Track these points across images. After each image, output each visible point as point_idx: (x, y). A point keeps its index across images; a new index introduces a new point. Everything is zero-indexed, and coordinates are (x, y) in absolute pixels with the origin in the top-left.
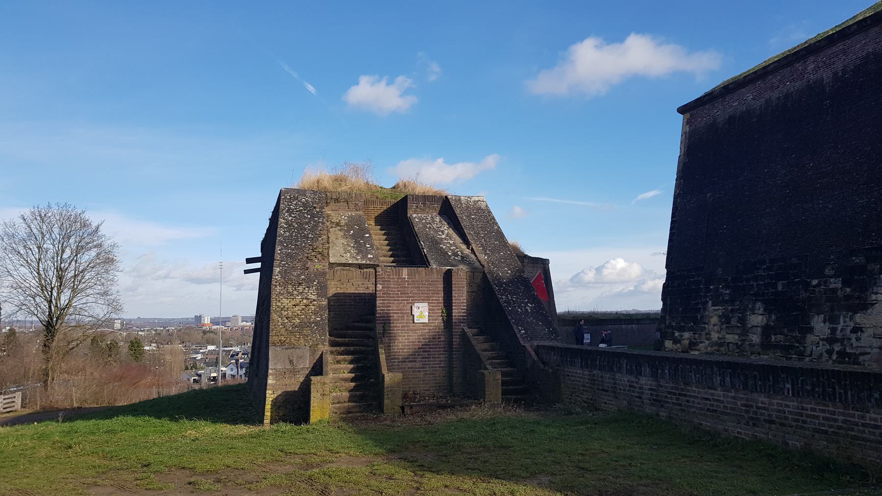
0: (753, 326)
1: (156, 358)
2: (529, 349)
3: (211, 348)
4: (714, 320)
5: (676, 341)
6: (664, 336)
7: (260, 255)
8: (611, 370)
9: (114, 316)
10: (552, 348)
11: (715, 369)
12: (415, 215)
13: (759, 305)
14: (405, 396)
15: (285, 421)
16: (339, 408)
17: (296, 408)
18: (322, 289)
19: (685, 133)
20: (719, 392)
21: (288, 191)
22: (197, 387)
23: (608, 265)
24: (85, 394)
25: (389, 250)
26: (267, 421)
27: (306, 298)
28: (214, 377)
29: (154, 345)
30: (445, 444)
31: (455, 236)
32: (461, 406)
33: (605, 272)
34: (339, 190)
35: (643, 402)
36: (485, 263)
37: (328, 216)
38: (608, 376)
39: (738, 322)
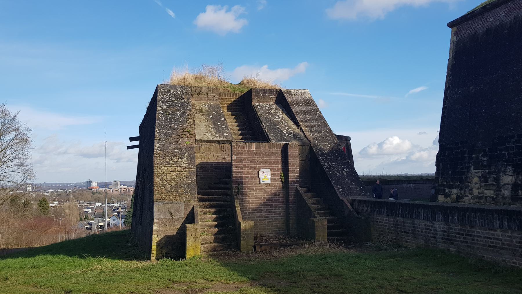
0: (505, 184)
1: (59, 213)
2: (346, 202)
3: (98, 204)
4: (476, 180)
5: (447, 196)
6: (438, 192)
7: (138, 135)
8: (411, 217)
9: (28, 181)
10: (364, 202)
11: (495, 215)
12: (257, 104)
13: (509, 168)
14: (255, 238)
15: (167, 257)
16: (207, 247)
17: (175, 247)
18: (191, 159)
19: (453, 42)
20: (499, 233)
21: (163, 86)
22: (91, 233)
23: (387, 142)
24: (9, 239)
25: (239, 130)
26: (153, 257)
27: (180, 166)
28: (101, 226)
29: (56, 202)
30: (292, 273)
31: (287, 119)
32: (298, 245)
33: (385, 146)
34: (200, 85)
35: (436, 241)
36: (311, 139)
37: (193, 105)
38: (409, 221)
39: (493, 181)
